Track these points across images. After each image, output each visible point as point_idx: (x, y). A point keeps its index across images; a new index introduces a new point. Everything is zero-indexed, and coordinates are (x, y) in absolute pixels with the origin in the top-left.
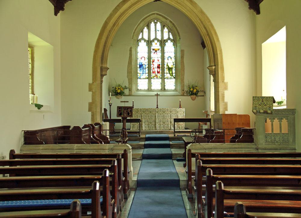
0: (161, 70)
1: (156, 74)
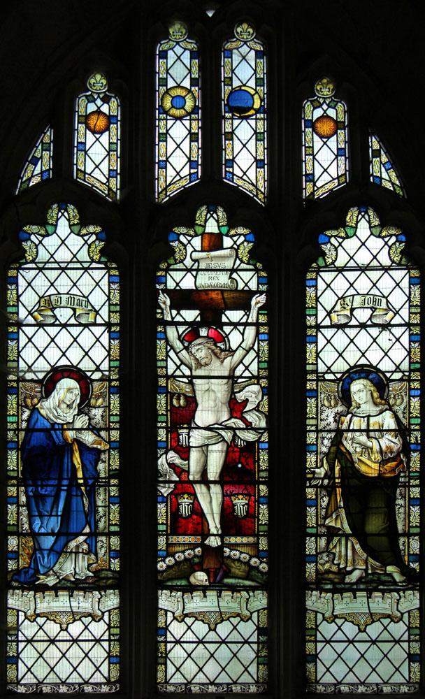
0: (271, 501)
1: (213, 542)
